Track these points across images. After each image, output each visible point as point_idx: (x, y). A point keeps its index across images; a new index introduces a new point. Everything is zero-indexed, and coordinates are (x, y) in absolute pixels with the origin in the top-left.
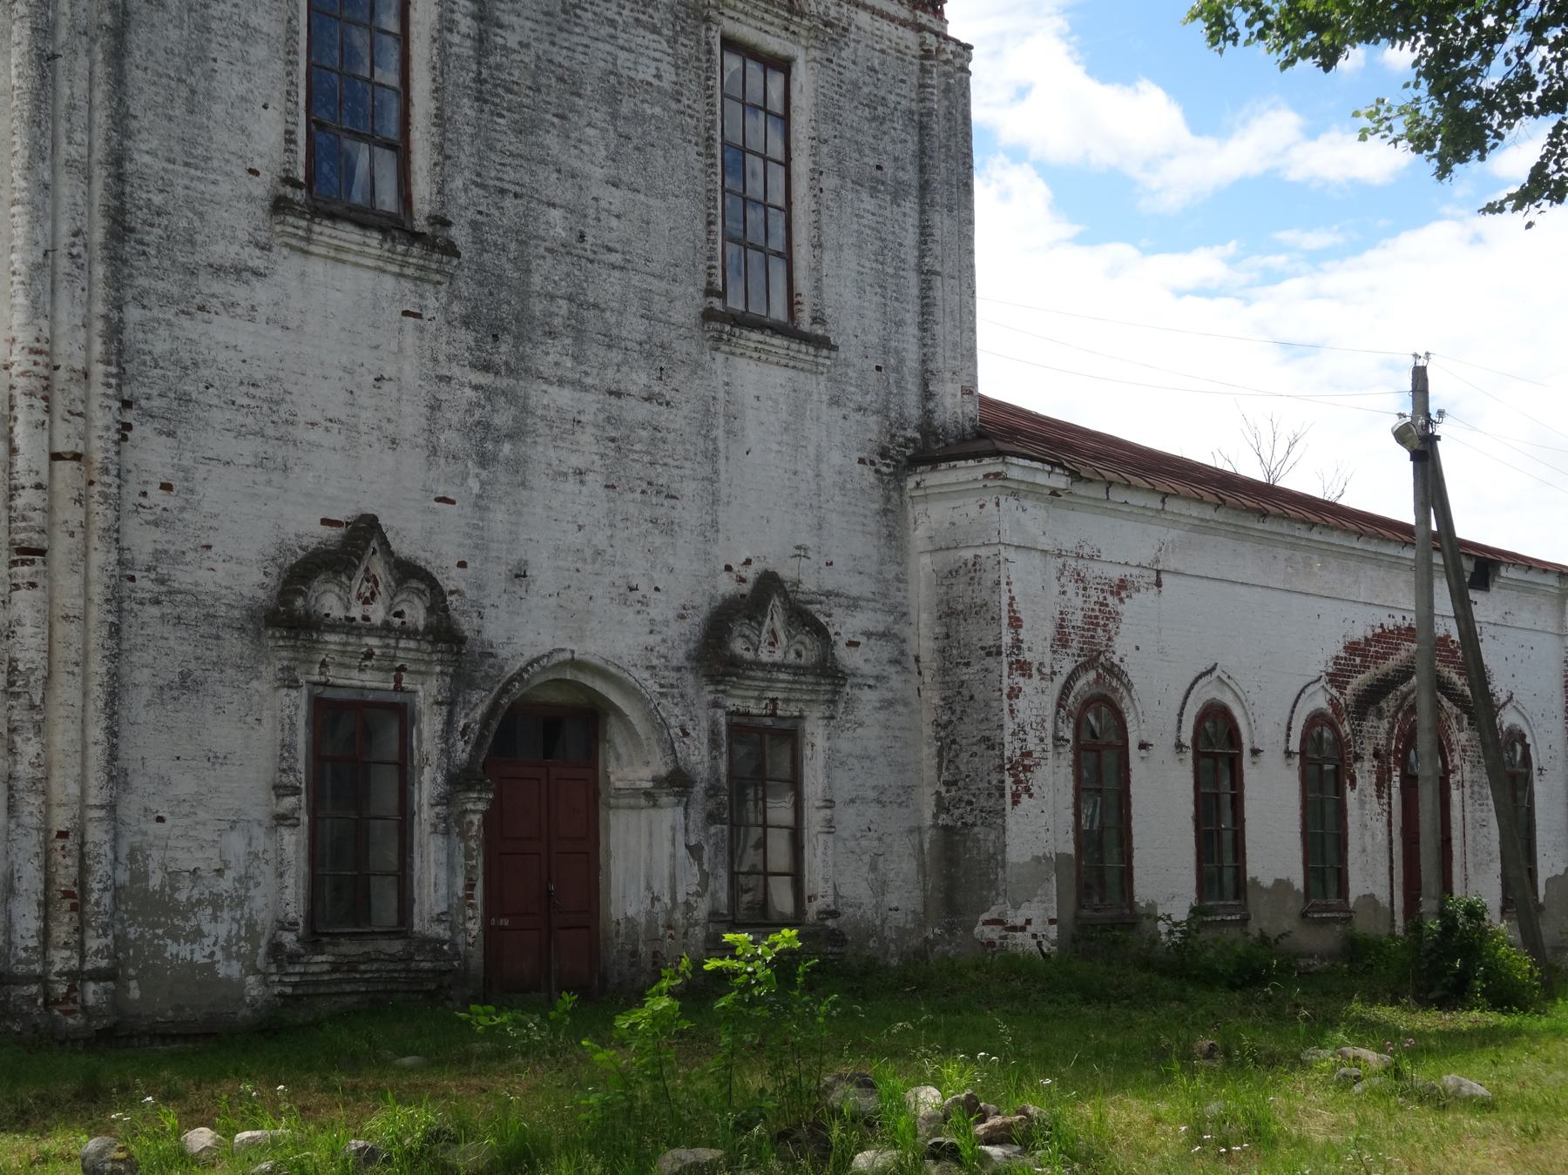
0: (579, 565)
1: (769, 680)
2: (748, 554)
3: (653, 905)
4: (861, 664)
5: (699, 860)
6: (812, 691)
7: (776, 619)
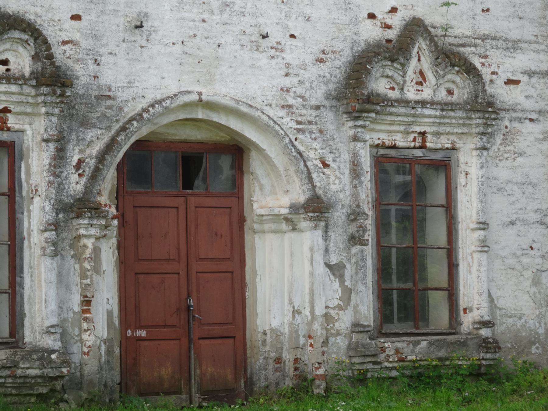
0: (205, 16)
1: (413, 116)
2: (394, 4)
3: (294, 317)
4: (521, 99)
5: (341, 278)
6: (464, 125)
7: (421, 58)
